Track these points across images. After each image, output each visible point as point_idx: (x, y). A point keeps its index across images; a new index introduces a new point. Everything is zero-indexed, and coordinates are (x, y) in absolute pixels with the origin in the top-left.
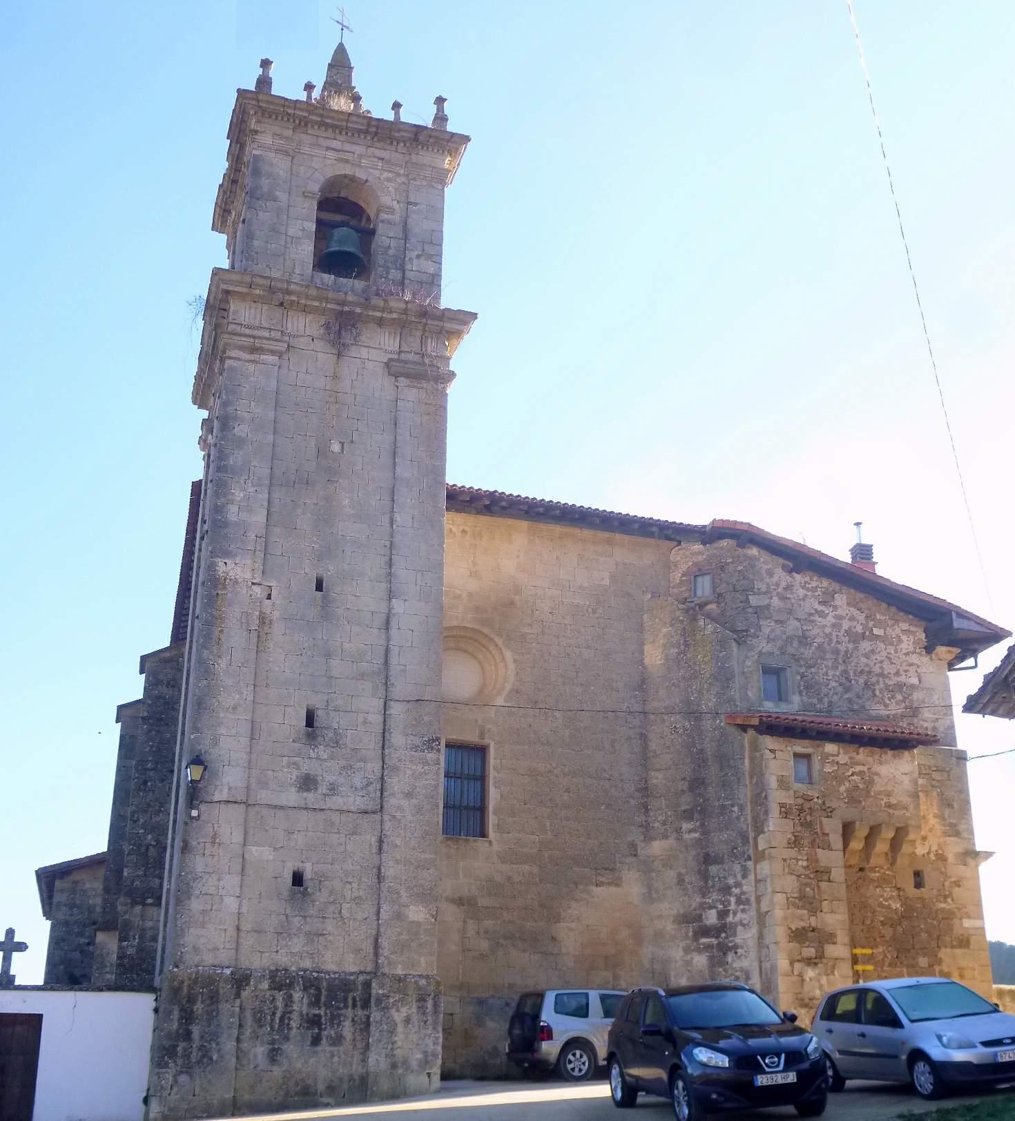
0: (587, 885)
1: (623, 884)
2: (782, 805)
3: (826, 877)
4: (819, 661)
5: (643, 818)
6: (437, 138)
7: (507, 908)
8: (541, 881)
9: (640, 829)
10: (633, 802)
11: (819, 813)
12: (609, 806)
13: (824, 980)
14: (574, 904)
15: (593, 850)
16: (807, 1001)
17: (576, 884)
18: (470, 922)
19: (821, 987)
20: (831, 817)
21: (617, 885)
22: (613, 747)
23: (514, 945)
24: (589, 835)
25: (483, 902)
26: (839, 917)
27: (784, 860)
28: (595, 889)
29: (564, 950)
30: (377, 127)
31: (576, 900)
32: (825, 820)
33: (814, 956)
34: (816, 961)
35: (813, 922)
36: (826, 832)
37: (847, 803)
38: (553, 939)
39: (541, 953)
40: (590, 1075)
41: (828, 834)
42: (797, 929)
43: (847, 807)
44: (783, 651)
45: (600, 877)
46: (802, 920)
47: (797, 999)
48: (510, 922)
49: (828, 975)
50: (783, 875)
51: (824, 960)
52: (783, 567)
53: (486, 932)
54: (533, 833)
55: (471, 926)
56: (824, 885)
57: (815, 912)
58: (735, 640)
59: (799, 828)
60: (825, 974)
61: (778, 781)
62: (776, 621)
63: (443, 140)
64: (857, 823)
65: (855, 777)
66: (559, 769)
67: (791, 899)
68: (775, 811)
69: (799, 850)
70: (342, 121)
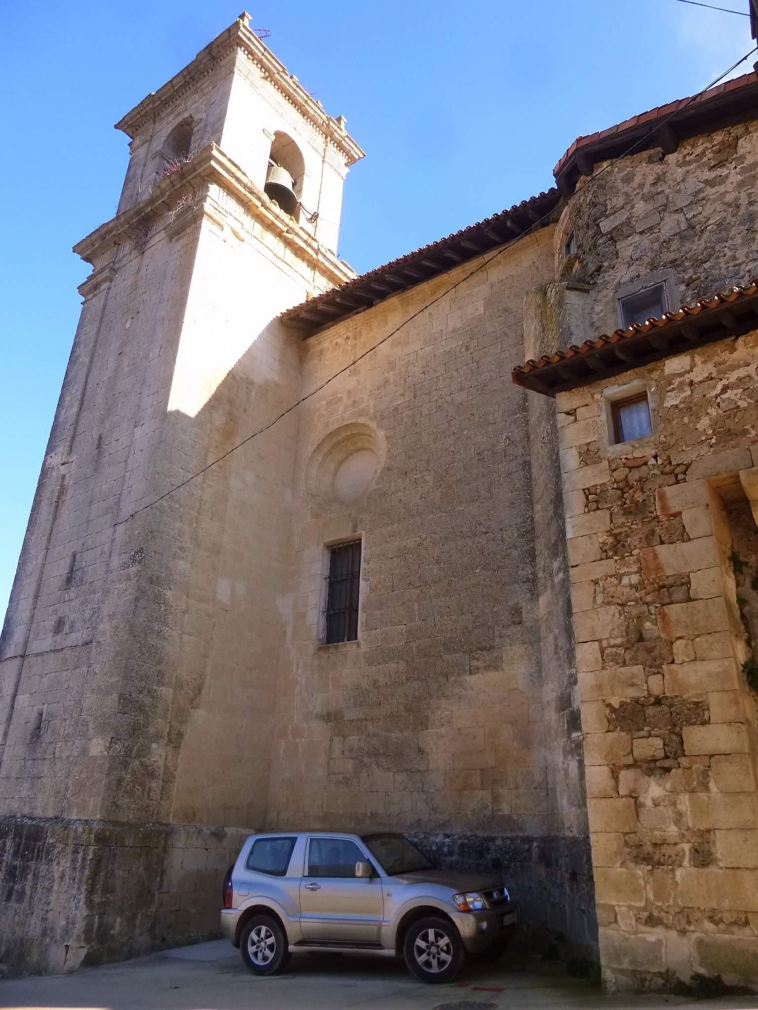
0: (459, 675)
1: (504, 665)
2: (587, 492)
3: (679, 595)
4: (717, 248)
5: (529, 569)
6: (222, 43)
7: (372, 719)
8: (407, 679)
9: (526, 586)
10: (515, 553)
11: (659, 481)
12: (485, 567)
13: (684, 803)
14: (443, 702)
15: (466, 628)
16: (648, 848)
17: (446, 676)
18: (336, 739)
19: (679, 818)
20: (684, 480)
21: (496, 668)
22: (490, 491)
23: (377, 763)
24: (462, 610)
25: (350, 714)
26: (712, 667)
27: (596, 582)
28: (468, 678)
29: (432, 766)
30: (189, 73)
31: (446, 697)
32: (669, 491)
33: (661, 754)
34: (667, 763)
35: (656, 684)
36: (673, 510)
37: (718, 443)
38: (420, 751)
39: (406, 771)
40: (276, 967)
41: (678, 514)
42: (622, 704)
43: (715, 452)
44: (653, 266)
45: (475, 661)
46: (633, 685)
47: (626, 844)
48: (375, 735)
49: (693, 791)
50: (594, 609)
51: (684, 761)
52: (650, 161)
53: (351, 750)
54: (400, 623)
55: (337, 743)
56: (674, 611)
57: (659, 666)
58: (568, 288)
59: (620, 520)
60: (686, 791)
61: (580, 454)
62: (641, 233)
63: (226, 40)
64: (742, 475)
65: (729, 394)
66: (429, 539)
67: (609, 650)
68: (574, 502)
69: (623, 558)
70: (170, 89)
